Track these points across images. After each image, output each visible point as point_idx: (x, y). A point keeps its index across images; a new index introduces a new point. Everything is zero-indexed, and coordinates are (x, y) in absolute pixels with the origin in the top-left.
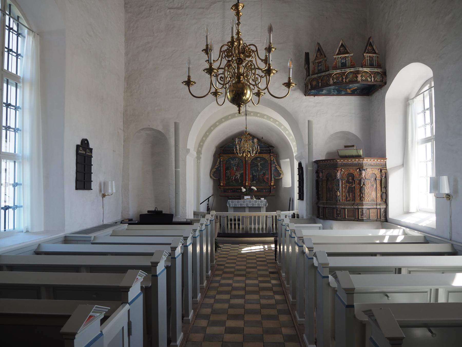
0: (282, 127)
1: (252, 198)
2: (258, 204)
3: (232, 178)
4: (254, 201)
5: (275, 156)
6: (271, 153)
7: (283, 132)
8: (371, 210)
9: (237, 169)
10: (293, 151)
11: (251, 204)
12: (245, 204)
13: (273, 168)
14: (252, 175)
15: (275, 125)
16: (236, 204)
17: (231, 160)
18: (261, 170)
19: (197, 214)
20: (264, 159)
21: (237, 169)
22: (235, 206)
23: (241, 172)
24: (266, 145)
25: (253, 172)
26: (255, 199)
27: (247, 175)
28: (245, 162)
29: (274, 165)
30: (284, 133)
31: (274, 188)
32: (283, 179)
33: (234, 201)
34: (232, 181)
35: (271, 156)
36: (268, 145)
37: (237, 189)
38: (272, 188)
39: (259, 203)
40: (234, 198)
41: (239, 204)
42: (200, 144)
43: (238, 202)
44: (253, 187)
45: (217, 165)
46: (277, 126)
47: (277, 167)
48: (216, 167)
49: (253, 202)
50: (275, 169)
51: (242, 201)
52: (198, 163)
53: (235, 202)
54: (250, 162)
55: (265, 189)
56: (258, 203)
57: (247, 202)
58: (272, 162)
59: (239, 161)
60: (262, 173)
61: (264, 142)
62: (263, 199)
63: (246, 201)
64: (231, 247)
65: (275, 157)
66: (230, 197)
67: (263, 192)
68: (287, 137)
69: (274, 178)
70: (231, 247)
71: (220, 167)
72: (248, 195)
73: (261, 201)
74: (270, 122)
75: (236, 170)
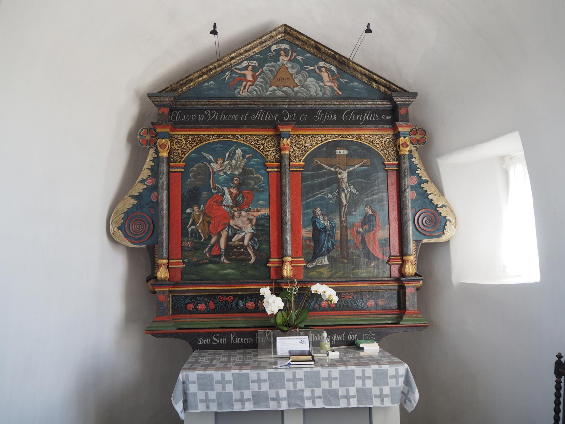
2: (358, 390)
3: (213, 240)
5: (418, 137)
8: (392, 255)
9: (240, 198)
11: (318, 392)
13: (410, 195)
14: (311, 228)
17: (211, 158)
21: (240, 198)
22: (220, 405)
23: (256, 214)
25: (314, 212)
27: (288, 227)
28: (280, 167)
32: (452, 246)
36: (382, 89)
37: (242, 297)
39: (369, 384)
40: (224, 341)
41: (247, 394)
44: (317, 288)
45: (143, 181)
47: (429, 187)
48: (138, 188)
51: (264, 374)
53: (223, 382)
54: (299, 166)
56: (359, 383)
58: (406, 165)
59: (249, 159)
60: (357, 217)
61: (365, 75)
66: (201, 341)
69: (417, 242)
71: (155, 188)
72: (295, 327)
75: (236, 203)
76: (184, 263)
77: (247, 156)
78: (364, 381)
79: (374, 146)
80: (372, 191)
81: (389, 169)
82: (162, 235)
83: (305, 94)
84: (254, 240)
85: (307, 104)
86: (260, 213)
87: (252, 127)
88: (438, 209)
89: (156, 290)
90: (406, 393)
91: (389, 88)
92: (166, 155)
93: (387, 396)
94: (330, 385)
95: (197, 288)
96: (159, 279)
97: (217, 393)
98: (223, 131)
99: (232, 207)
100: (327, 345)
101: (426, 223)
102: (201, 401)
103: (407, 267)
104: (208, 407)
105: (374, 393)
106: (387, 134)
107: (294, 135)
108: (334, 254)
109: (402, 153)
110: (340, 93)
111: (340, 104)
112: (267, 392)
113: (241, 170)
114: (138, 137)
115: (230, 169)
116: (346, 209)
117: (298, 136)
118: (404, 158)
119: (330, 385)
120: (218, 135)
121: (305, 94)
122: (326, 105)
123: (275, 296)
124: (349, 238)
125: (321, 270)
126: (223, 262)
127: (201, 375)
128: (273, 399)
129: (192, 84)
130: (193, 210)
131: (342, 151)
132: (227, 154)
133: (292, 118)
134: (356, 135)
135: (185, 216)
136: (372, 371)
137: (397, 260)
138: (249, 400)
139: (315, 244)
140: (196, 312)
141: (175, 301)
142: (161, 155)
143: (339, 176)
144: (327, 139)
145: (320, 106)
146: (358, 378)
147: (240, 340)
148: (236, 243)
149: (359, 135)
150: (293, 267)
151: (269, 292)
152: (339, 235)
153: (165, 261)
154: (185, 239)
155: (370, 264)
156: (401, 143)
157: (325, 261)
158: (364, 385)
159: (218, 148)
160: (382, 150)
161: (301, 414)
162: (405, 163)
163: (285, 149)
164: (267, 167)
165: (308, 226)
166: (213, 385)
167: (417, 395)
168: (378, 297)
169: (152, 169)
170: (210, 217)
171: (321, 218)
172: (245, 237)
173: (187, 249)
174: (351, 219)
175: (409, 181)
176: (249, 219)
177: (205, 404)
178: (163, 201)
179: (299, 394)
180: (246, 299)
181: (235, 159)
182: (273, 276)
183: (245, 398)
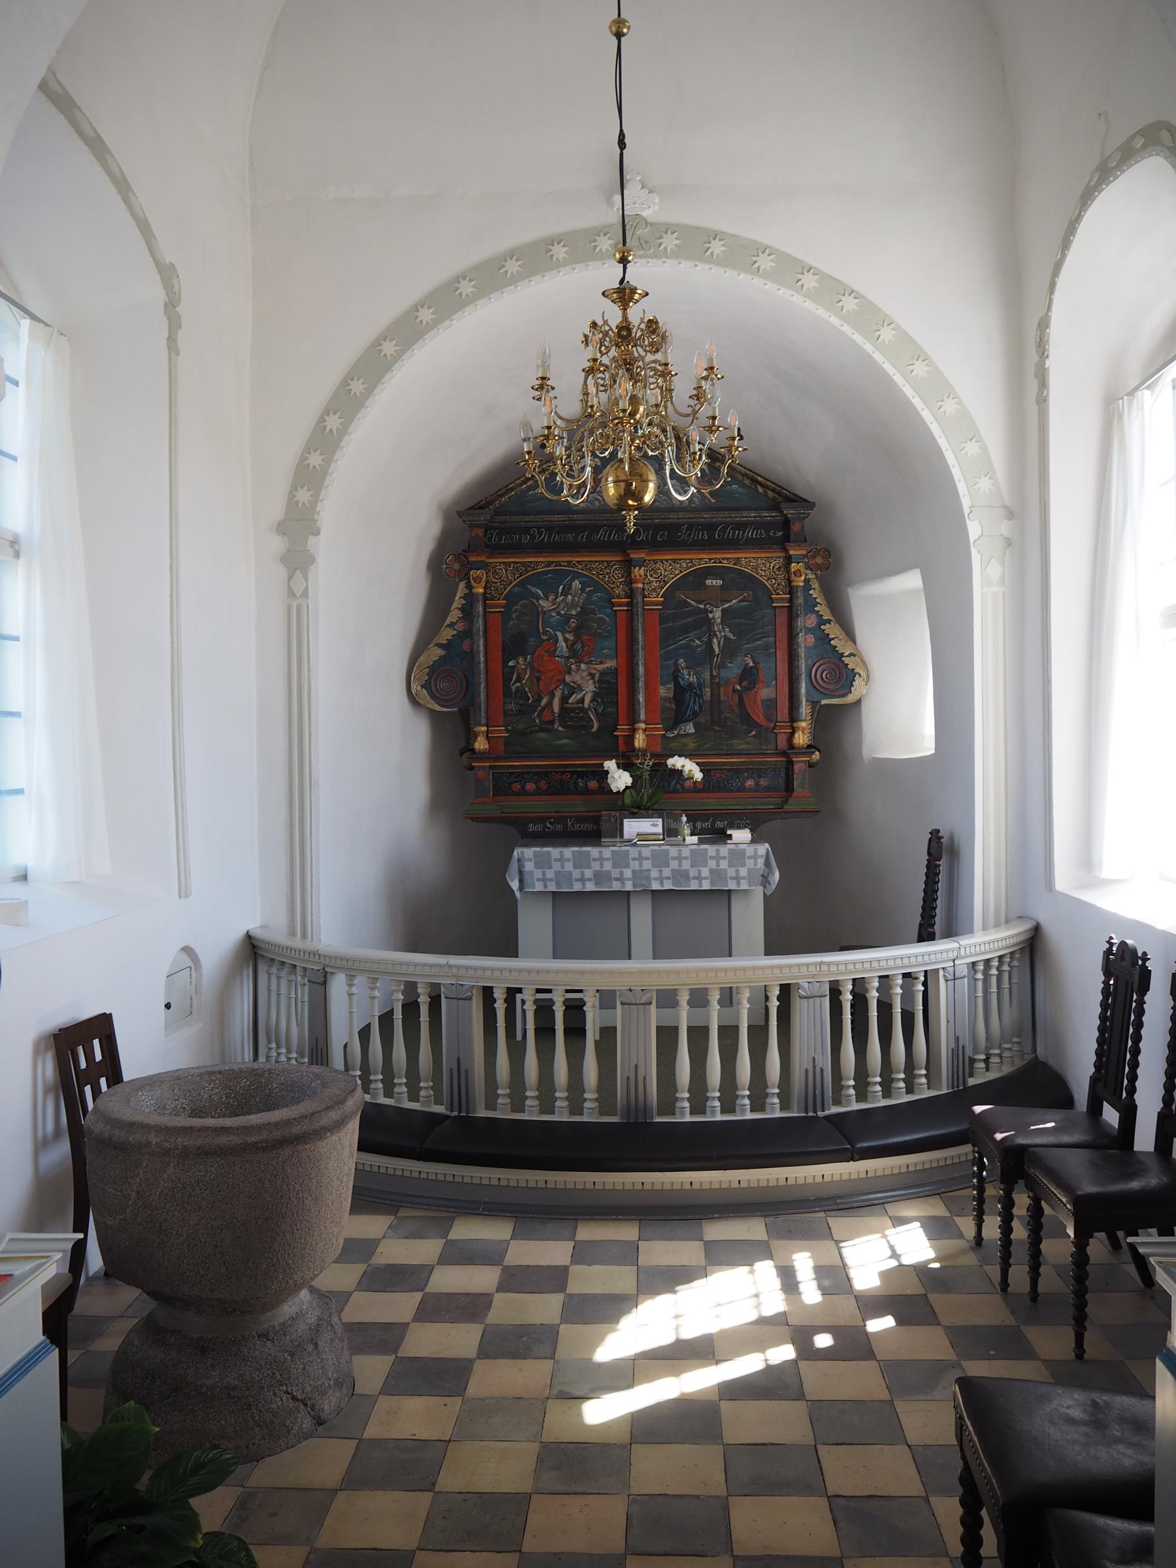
0: (887, 334)
1: (670, 832)
2: (711, 871)
3: (544, 701)
4: (686, 852)
5: (819, 560)
6: (789, 541)
7: (887, 367)
9: (578, 646)
10: (966, 503)
11: (667, 872)
12: (628, 873)
13: (805, 641)
14: (671, 686)
15: (834, 320)
16: (570, 873)
18: (730, 650)
19: (283, 963)
20: (747, 581)
21: (578, 646)
22: (558, 884)
23: (600, 667)
24: (760, 490)
25: (676, 664)
26: (695, 839)
27: (641, 684)
28: (630, 604)
29: (811, 621)
30: (898, 379)
31: (811, 765)
32: (865, 708)
33: (554, 852)
34: (547, 726)
35: (789, 560)
36: (771, 494)
37: (582, 775)
38: (797, 767)
39: (724, 864)
40: (559, 827)
41: (588, 873)
42: (303, 458)
43: (581, 862)
44: (677, 762)
45: (452, 625)
46: (846, 329)
47: (832, 630)
48: (446, 634)
49: (680, 858)
50: (815, 647)
51: (607, 852)
52: (291, 594)
53: (561, 860)
54: (656, 604)
55: (757, 772)
56: (712, 864)
57: (640, 858)
58: (800, 600)
60: (732, 671)
62: (741, 836)
63: (633, 852)
64: (504, 1286)
65: (819, 567)
66: (532, 827)
67: (742, 789)
68: (917, 402)
69: (814, 704)
70: (504, 1286)
71: (468, 634)
72: (647, 809)
73: (731, 852)
74: (797, 298)
75: (573, 653)
76: (507, 731)
77: (588, 589)
78: (718, 862)
79: (757, 573)
80: (754, 636)
81: (778, 605)
82: (480, 696)
83: (664, 503)
84: (597, 702)
85: (666, 519)
86: (604, 666)
87: (593, 552)
88: (843, 659)
89: (473, 764)
90: (766, 875)
91: (779, 494)
92: (481, 590)
93: (743, 878)
94: (680, 865)
95: (525, 763)
96: (477, 751)
97: (555, 872)
98: (554, 556)
99: (568, 658)
100: (687, 831)
101: (827, 678)
102: (538, 880)
103: (796, 736)
104: (545, 886)
105: (729, 875)
106: (777, 557)
107: (649, 561)
108: (702, 719)
109: (794, 584)
110: (713, 501)
111: (712, 518)
112: (610, 871)
113: (579, 609)
114: (444, 566)
115: (564, 608)
116: (719, 659)
117: (655, 562)
118: (797, 592)
119: (680, 865)
120: (548, 562)
121: (664, 503)
122: (693, 518)
123: (621, 771)
124: (722, 698)
125: (685, 740)
126: (557, 730)
127: (538, 852)
128: (616, 879)
129: (513, 493)
130: (518, 663)
131: (714, 581)
132: (561, 587)
133: (647, 536)
134: (734, 559)
135: (506, 670)
136: (727, 851)
137: (786, 726)
138: (590, 880)
139: (676, 706)
140: (523, 793)
141: (496, 777)
142: (475, 591)
143: (711, 615)
144: (694, 566)
145: (685, 520)
146: (711, 858)
147: (580, 827)
148: (573, 706)
149: (738, 559)
150: (647, 736)
151: (615, 766)
152: (709, 694)
153: (484, 729)
154: (508, 700)
155: (750, 733)
156: (793, 570)
157: (690, 728)
158: (718, 865)
159: (549, 578)
160: (768, 579)
161: (650, 896)
162: (797, 598)
163: (637, 581)
164: (613, 605)
165: (668, 683)
166: (551, 863)
167: (777, 876)
168: (759, 777)
169: (462, 609)
170: (538, 671)
171: (685, 672)
172: (586, 698)
173: (512, 713)
174: (724, 674)
175: (806, 621)
176: (590, 674)
177: (542, 883)
178: (479, 652)
179: (646, 873)
180: (587, 777)
181: (571, 594)
182: (622, 748)
183: (586, 877)
